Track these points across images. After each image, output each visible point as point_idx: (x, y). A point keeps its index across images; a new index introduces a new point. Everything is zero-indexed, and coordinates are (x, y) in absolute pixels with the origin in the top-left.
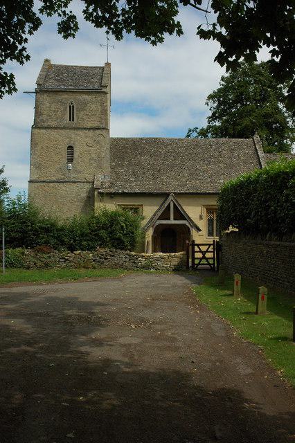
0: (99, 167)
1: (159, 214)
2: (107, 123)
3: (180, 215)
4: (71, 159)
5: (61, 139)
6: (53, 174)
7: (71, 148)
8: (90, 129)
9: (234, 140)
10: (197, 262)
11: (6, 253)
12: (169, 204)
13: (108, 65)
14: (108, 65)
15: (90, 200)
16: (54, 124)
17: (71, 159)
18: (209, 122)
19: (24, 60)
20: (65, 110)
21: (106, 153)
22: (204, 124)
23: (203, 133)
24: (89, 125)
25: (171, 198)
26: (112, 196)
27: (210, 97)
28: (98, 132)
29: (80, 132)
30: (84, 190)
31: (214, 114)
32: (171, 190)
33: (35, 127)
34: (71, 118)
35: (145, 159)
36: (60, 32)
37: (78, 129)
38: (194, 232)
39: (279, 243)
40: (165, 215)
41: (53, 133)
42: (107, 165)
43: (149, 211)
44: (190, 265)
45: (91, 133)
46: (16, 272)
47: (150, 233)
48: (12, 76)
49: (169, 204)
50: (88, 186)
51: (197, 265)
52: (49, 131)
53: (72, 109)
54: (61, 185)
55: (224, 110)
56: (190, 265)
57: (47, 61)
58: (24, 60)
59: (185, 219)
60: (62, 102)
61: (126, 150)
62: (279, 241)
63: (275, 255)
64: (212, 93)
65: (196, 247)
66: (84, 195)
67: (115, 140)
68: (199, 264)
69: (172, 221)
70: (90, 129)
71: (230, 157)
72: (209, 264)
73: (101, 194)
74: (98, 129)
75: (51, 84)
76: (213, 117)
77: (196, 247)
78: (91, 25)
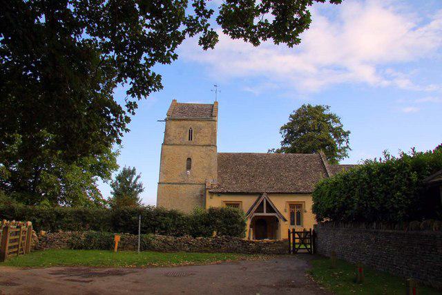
0: (210, 173)
1: (255, 208)
2: (216, 142)
3: (271, 209)
4: (189, 167)
5: (183, 153)
6: (176, 178)
7: (189, 159)
8: (203, 146)
9: (306, 155)
10: (297, 246)
11: (141, 237)
12: (263, 201)
13: (216, 103)
14: (216, 103)
15: (202, 198)
16: (178, 142)
17: (189, 167)
18: (282, 145)
19: (171, 60)
20: (186, 132)
21: (214, 164)
22: (280, 147)
23: (278, 151)
24: (203, 143)
25: (264, 196)
26: (219, 194)
27: (282, 128)
28: (209, 148)
29: (196, 148)
30: (196, 190)
31: (285, 140)
32: (263, 190)
33: (164, 144)
34: (190, 138)
35: (243, 168)
36: (200, 44)
37: (194, 145)
38: (281, 221)
39: (391, 231)
40: (260, 209)
41: (177, 149)
42: (215, 173)
43: (247, 203)
44: (292, 249)
45: (204, 149)
46: (151, 255)
47: (248, 222)
48: (159, 77)
49: (263, 201)
50: (200, 187)
51: (298, 249)
52: (174, 147)
53: (191, 132)
54: (181, 186)
55: (292, 137)
56: (292, 249)
57: (174, 101)
58: (171, 60)
59: (275, 212)
60: (184, 127)
61: (229, 162)
62: (391, 229)
63: (389, 242)
64: (283, 125)
65: (296, 234)
66: (198, 194)
67: (221, 154)
68: (299, 248)
69: (265, 214)
70: (203, 146)
71: (304, 167)
72: (307, 248)
73: (211, 193)
74: (210, 146)
75: (177, 116)
76: (285, 142)
77: (296, 234)
78: (228, 37)
